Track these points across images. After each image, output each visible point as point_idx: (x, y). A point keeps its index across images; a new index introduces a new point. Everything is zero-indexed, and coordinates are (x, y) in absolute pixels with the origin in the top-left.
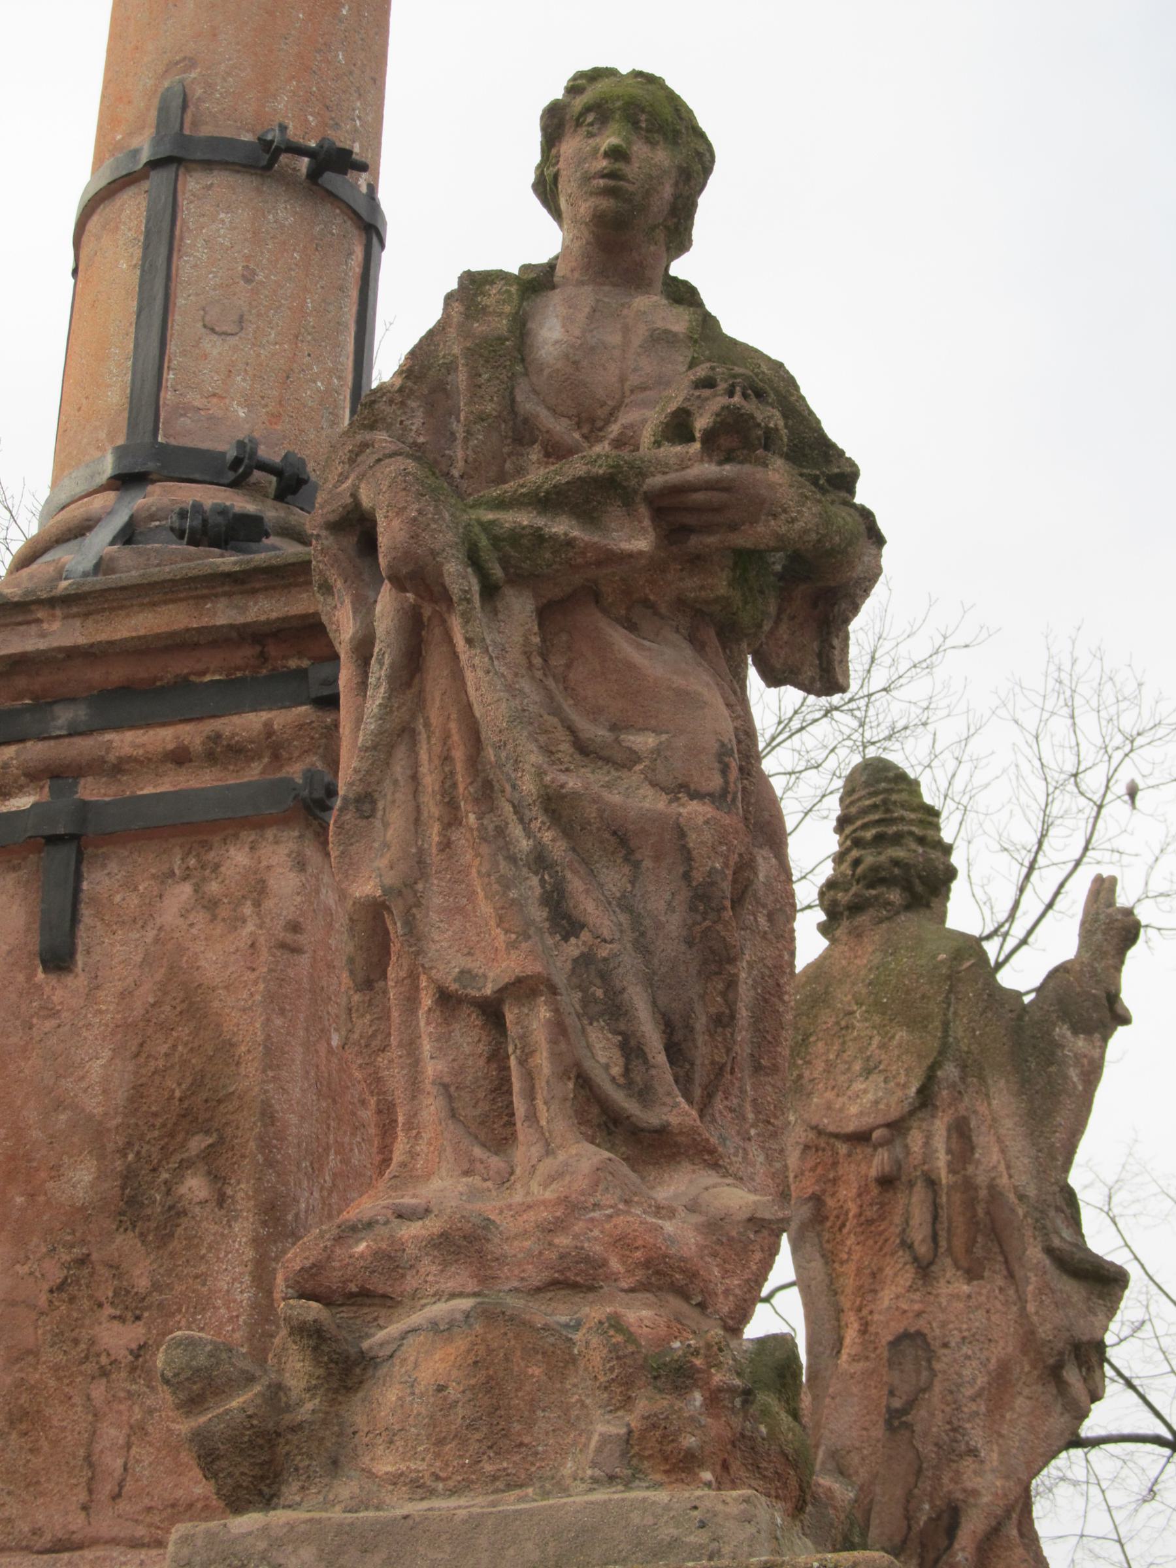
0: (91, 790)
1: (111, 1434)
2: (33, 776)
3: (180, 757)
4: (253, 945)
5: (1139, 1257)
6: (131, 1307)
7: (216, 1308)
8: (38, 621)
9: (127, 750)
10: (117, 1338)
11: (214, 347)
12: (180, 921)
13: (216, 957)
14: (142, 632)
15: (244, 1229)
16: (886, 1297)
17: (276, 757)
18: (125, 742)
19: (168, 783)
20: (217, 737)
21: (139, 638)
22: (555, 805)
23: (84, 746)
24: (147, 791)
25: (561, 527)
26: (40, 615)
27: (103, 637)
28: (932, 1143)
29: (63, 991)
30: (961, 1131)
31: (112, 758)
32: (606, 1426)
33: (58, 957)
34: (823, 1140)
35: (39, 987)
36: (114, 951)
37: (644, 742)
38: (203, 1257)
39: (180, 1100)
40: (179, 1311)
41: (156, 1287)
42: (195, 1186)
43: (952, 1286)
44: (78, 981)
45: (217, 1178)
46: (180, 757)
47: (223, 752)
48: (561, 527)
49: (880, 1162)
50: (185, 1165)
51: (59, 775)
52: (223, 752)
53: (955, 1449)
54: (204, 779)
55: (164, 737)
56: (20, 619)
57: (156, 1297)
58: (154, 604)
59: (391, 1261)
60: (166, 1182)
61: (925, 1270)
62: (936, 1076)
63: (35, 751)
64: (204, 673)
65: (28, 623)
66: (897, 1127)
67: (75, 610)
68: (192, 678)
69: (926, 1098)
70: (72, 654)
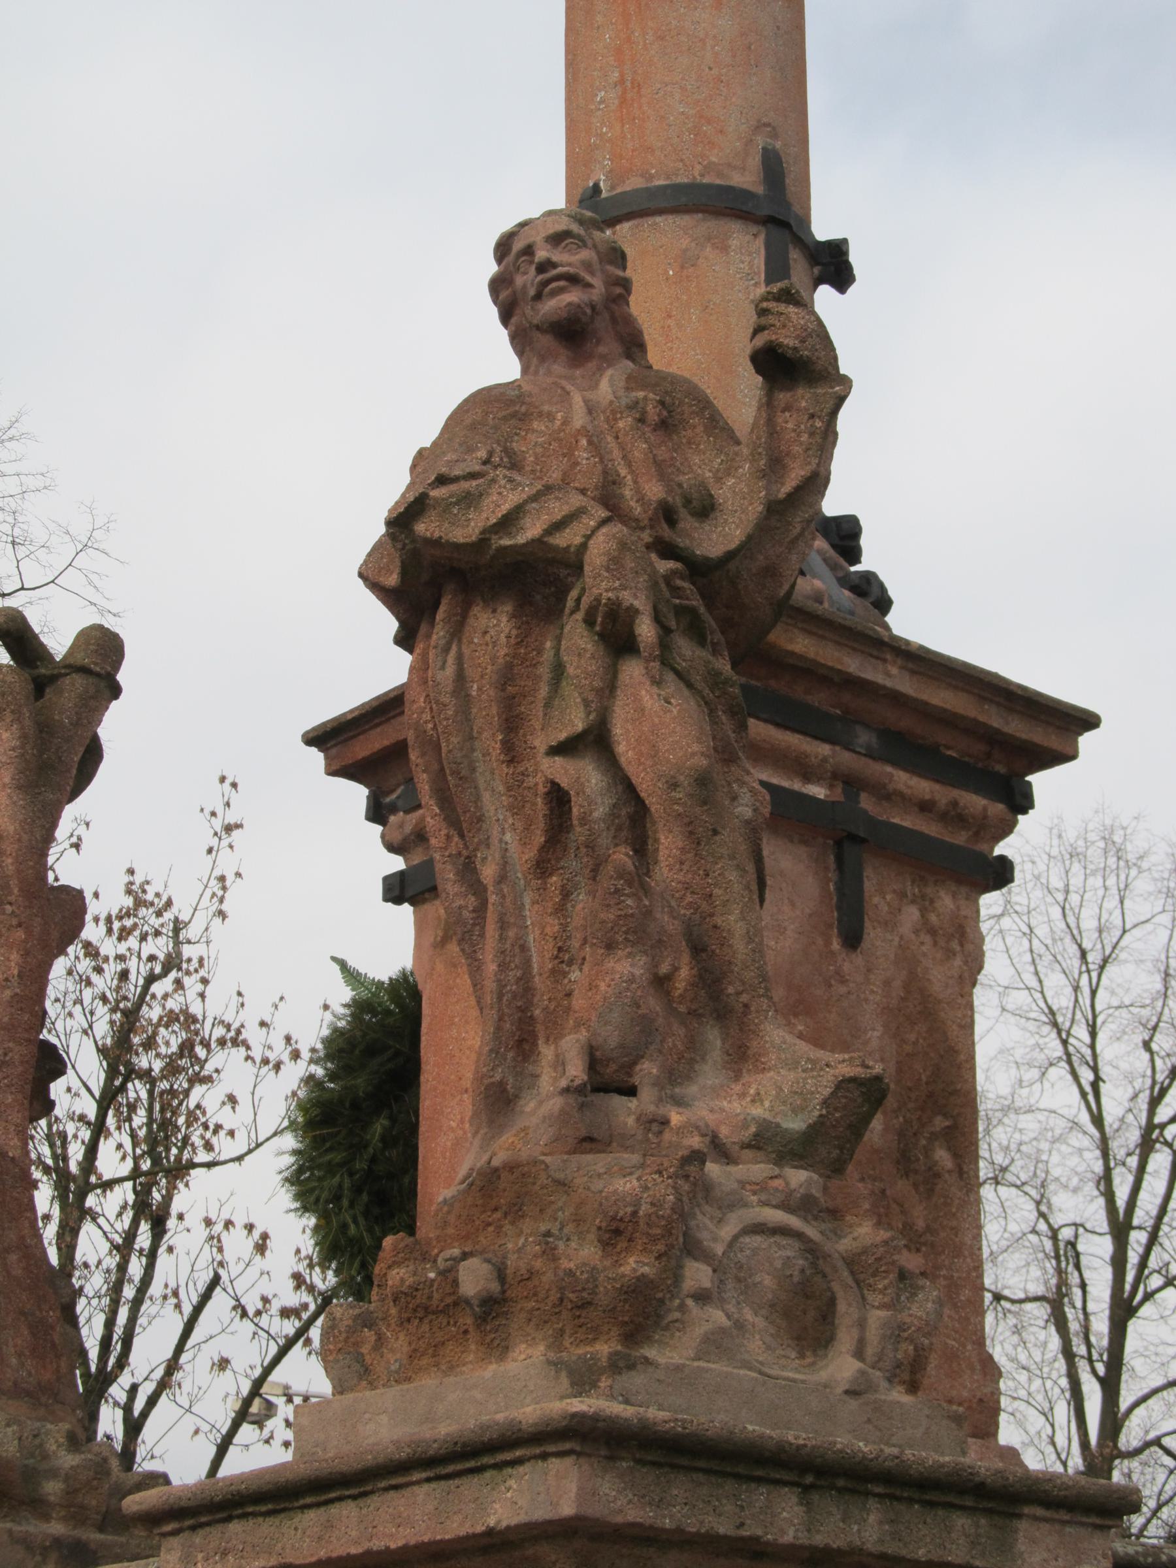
0: (866, 802)
4: (960, 977)
5: (261, 1148)
7: (965, 1257)
8: (885, 661)
9: (901, 787)
12: (913, 936)
14: (948, 706)
17: (977, 834)
18: (903, 780)
20: (955, 804)
21: (945, 710)
24: (896, 820)
26: (888, 657)
27: (924, 697)
29: (852, 964)
31: (891, 787)
33: (853, 939)
35: (832, 953)
38: (954, 1215)
39: (927, 1083)
40: (943, 1252)
41: (928, 1229)
44: (858, 959)
46: (925, 807)
50: (934, 1136)
51: (851, 783)
52: (955, 817)
54: (931, 828)
55: (922, 787)
56: (875, 653)
57: (928, 1237)
58: (956, 688)
60: (924, 1147)
63: (845, 759)
64: (949, 748)
65: (877, 658)
67: (910, 665)
68: (941, 748)
70: (896, 698)
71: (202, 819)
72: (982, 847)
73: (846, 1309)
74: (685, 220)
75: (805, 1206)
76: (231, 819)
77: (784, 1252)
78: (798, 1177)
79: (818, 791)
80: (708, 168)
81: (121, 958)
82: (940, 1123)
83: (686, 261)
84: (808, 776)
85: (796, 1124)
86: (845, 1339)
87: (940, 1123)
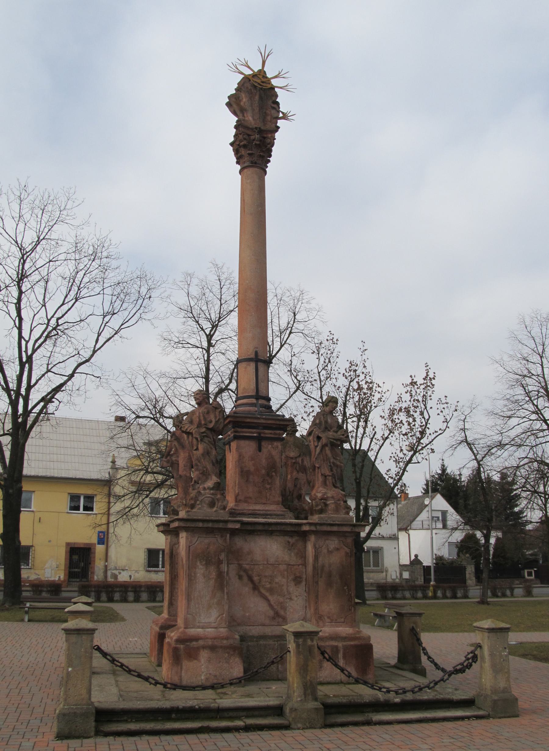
0: (262, 435)
1: (268, 495)
2: (257, 433)
3: (271, 434)
6: (269, 484)
10: (268, 486)
11: (262, 384)
13: (274, 453)
15: (278, 478)
16: (294, 474)
18: (266, 431)
19: (269, 436)
22: (333, 463)
23: (262, 431)
25: (335, 441)
28: (299, 460)
29: (260, 454)
30: (302, 460)
32: (344, 511)
33: (260, 450)
34: (287, 457)
36: (264, 450)
37: (338, 458)
42: (274, 474)
43: (301, 474)
45: (275, 473)
46: (271, 434)
47: (275, 434)
48: (335, 441)
49: (294, 461)
51: (260, 434)
52: (275, 434)
53: (300, 489)
54: (273, 436)
55: (270, 431)
59: (328, 497)
61: (298, 472)
62: (234, 414)
63: (258, 431)
66: (296, 458)
69: (299, 456)
71: (359, 350)
72: (281, 436)
73: (216, 503)
74: (245, 363)
75: (213, 494)
76: (365, 348)
77: (210, 499)
78: (212, 491)
79: (255, 435)
80: (248, 355)
81: (350, 376)
82: (273, 470)
83: (246, 368)
84: (253, 433)
85: (212, 487)
86: (216, 506)
87: (273, 470)
